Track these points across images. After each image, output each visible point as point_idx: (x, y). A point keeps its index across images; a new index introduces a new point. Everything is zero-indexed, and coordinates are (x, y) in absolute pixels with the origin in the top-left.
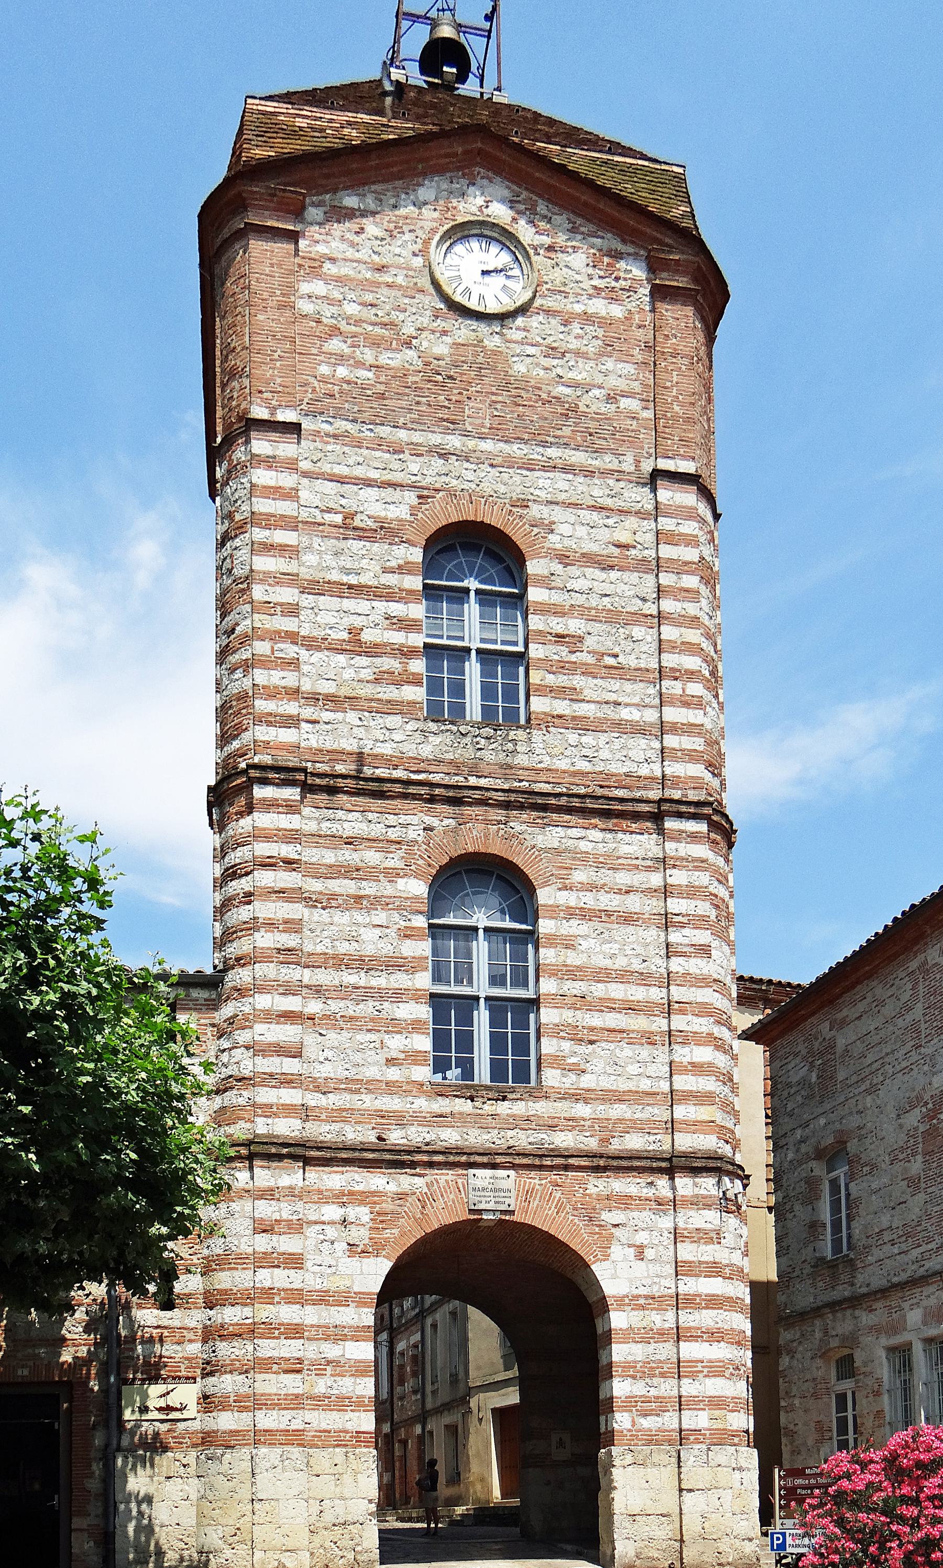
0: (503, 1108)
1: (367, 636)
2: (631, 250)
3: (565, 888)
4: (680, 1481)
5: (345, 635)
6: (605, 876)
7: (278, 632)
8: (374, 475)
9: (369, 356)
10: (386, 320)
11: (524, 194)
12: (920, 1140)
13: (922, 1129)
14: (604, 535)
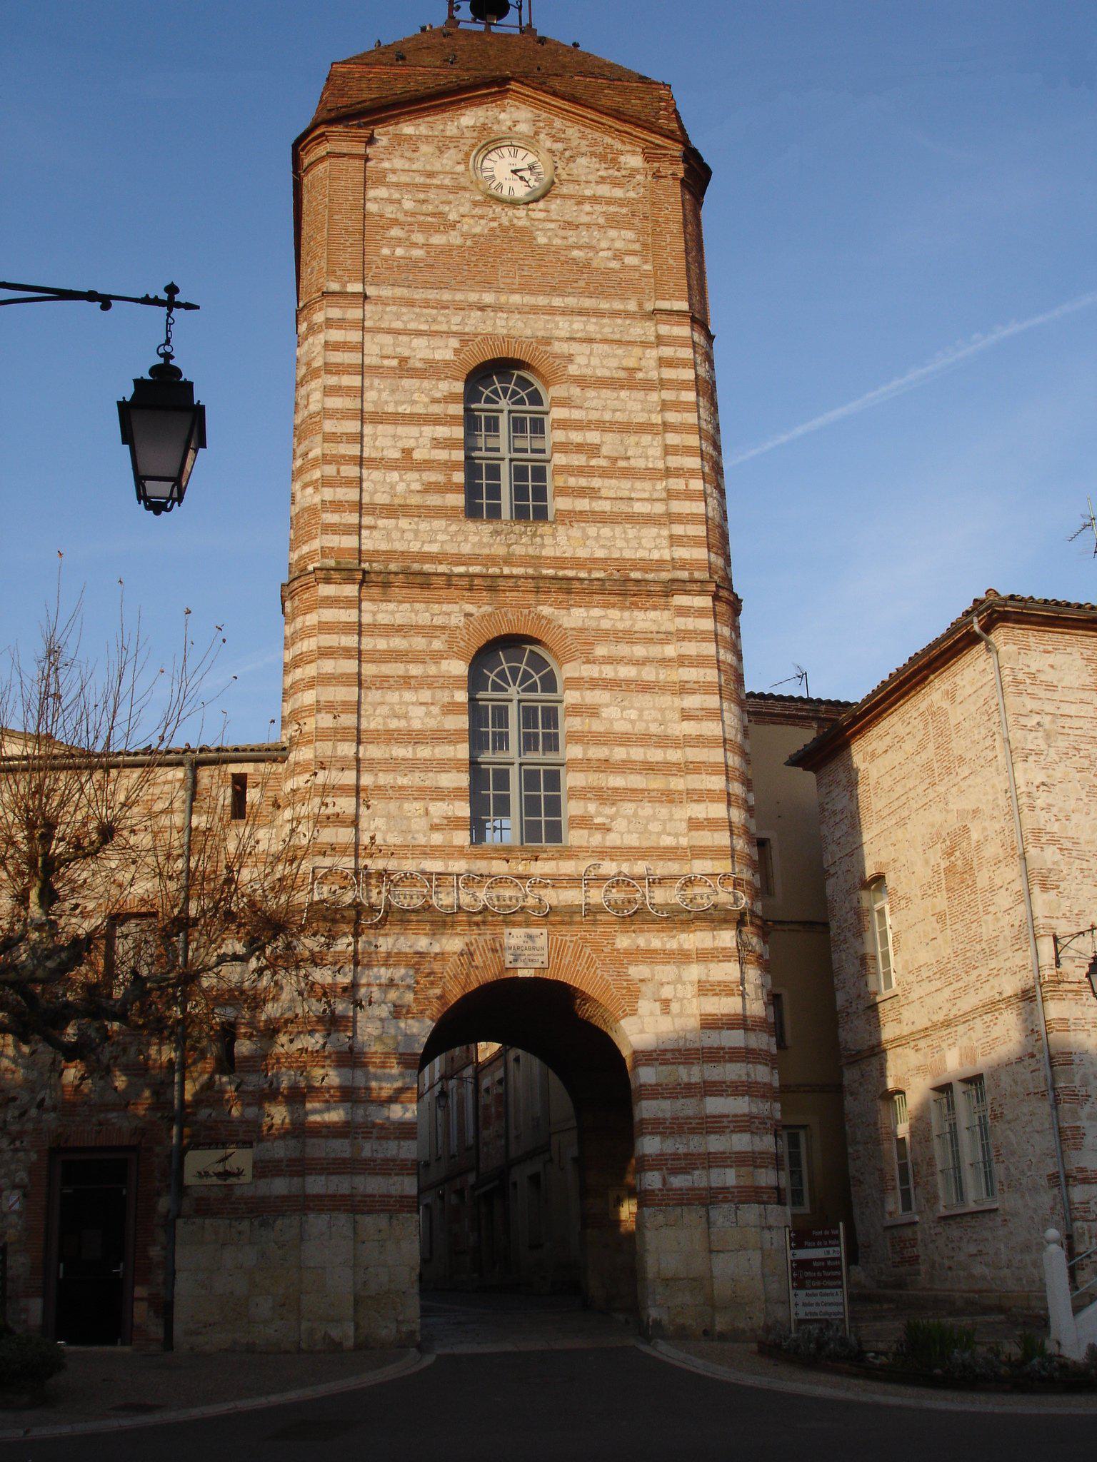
0: (538, 868)
1: (417, 455)
2: (628, 148)
3: (588, 662)
4: (710, 1243)
5: (397, 455)
6: (623, 650)
7: (343, 456)
8: (424, 327)
9: (419, 238)
10: (436, 210)
11: (544, 115)
12: (943, 875)
13: (943, 866)
14: (613, 363)
